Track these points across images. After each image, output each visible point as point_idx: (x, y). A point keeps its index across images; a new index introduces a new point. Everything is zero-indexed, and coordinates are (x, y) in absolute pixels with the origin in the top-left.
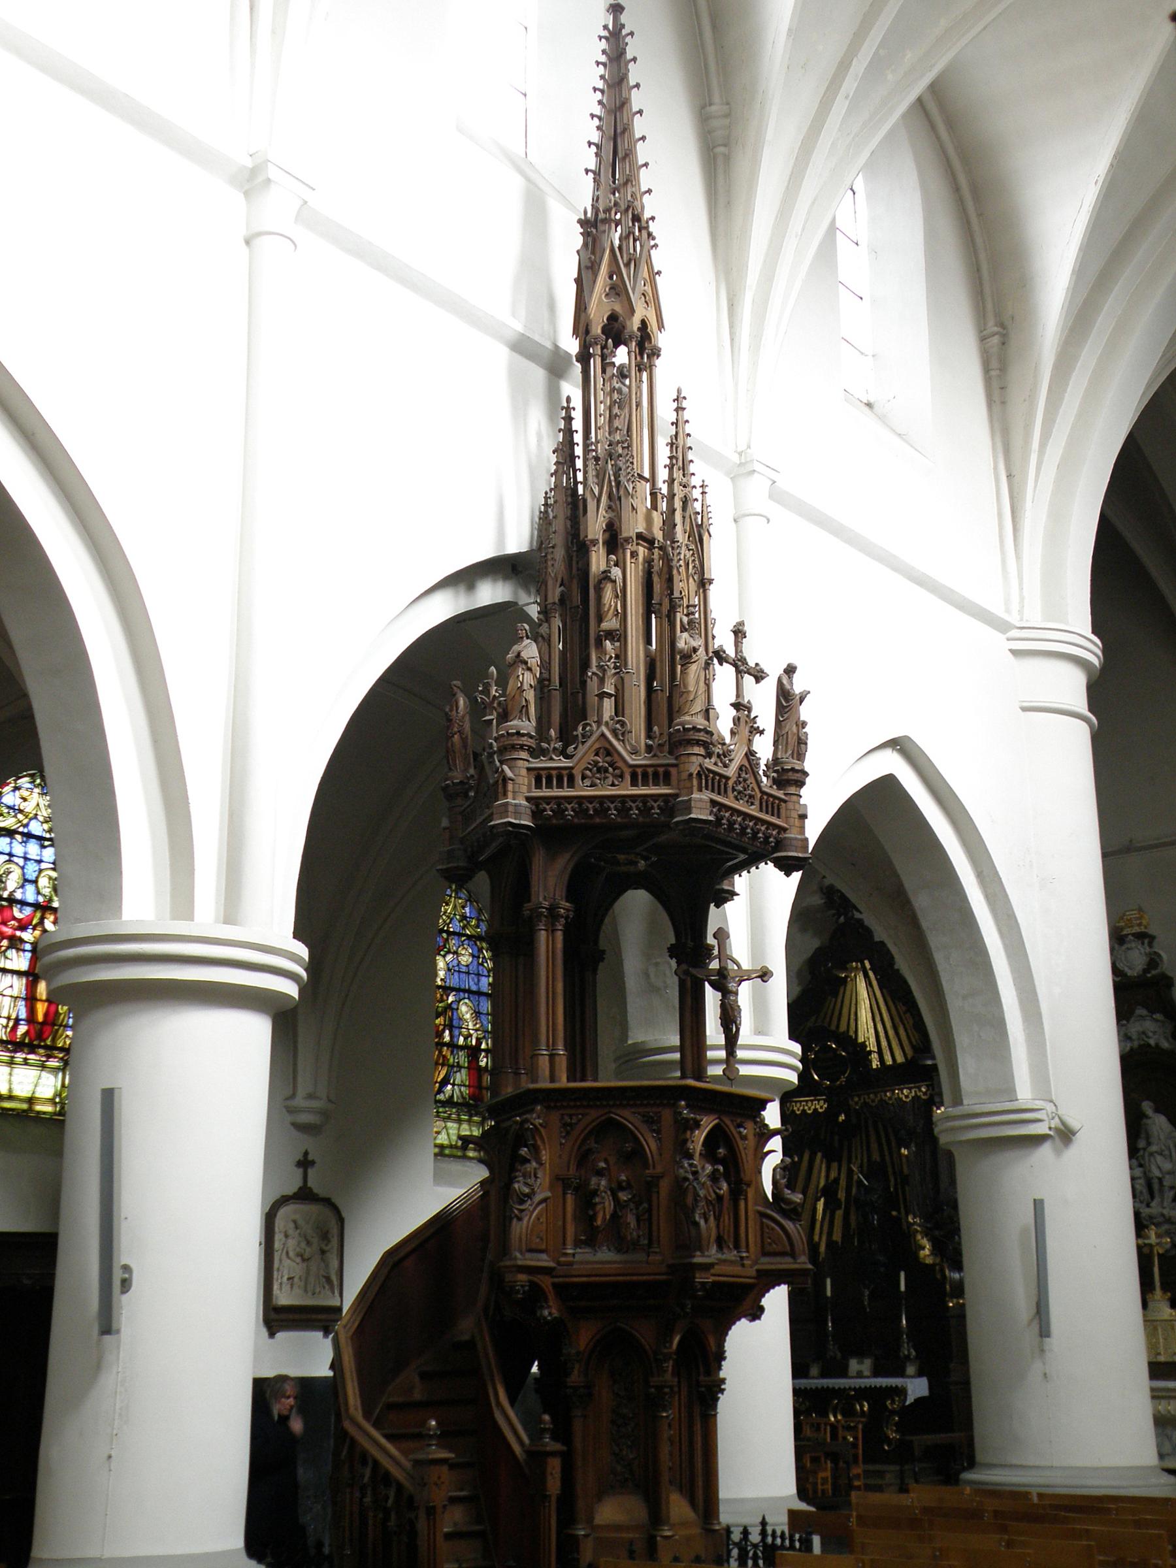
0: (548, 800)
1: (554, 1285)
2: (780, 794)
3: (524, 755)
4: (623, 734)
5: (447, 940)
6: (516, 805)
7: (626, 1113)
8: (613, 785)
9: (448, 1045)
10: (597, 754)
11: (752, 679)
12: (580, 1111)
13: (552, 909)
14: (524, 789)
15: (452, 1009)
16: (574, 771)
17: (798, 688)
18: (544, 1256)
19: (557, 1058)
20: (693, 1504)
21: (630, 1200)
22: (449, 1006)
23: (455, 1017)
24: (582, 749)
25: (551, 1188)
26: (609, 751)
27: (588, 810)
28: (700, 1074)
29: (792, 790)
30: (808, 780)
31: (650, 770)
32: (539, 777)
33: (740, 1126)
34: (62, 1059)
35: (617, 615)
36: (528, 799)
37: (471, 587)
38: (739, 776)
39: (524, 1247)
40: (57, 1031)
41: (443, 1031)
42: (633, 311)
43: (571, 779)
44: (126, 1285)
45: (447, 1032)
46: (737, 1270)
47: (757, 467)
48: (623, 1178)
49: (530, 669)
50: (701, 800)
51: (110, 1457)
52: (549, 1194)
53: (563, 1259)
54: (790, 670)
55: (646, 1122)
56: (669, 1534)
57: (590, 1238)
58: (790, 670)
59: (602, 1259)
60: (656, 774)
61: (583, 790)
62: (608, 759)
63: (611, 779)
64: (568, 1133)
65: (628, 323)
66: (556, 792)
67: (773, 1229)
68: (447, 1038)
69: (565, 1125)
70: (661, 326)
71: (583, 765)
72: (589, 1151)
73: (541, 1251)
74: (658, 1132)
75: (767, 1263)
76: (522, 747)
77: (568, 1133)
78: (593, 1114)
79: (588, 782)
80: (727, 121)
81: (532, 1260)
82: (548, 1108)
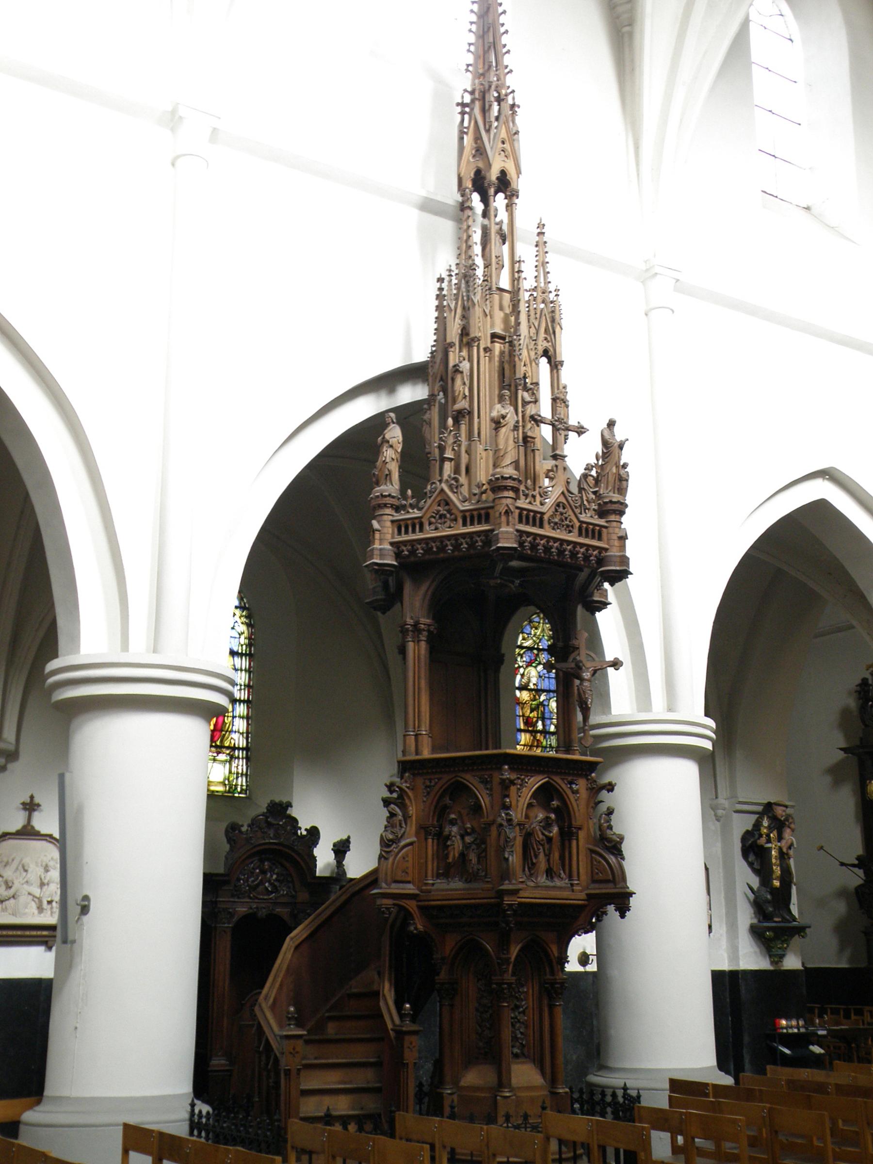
0: (404, 543)
1: (419, 907)
2: (602, 522)
3: (388, 511)
4: (457, 488)
5: (537, 655)
6: (381, 550)
7: (468, 776)
8: (450, 527)
9: (541, 732)
10: (439, 505)
11: (576, 434)
12: (437, 776)
13: (416, 625)
14: (389, 537)
15: (544, 706)
16: (423, 520)
17: (619, 436)
18: (411, 886)
19: (420, 737)
20: (543, 1074)
21: (473, 842)
22: (541, 704)
23: (546, 711)
24: (429, 501)
25: (417, 834)
26: (447, 502)
27: (432, 547)
29: (613, 517)
30: (627, 510)
31: (475, 513)
32: (400, 526)
33: (571, 783)
34: (229, 754)
35: (465, 397)
36: (392, 544)
37: (392, 391)
38: (556, 511)
39: (389, 878)
40: (224, 735)
41: (537, 722)
42: (489, 166)
43: (421, 526)
44: (85, 910)
45: (540, 723)
46: (566, 894)
47: (657, 270)
48: (469, 826)
49: (391, 446)
50: (507, 532)
51: (76, 1028)
52: (414, 839)
53: (424, 888)
54: (611, 424)
55: (482, 782)
56: (508, 1094)
57: (446, 872)
58: (611, 424)
59: (452, 888)
60: (480, 516)
61: (547, 531)
62: (447, 507)
63: (448, 522)
64: (428, 793)
65: (488, 175)
66: (411, 537)
67: (599, 862)
68: (540, 726)
69: (427, 787)
70: (519, 172)
71: (428, 515)
72: (445, 807)
73: (409, 882)
74: (491, 789)
75: (596, 889)
76: (385, 505)
77: (428, 793)
78: (446, 778)
79: (433, 527)
80: (629, 6)
81: (395, 889)
82: (414, 775)
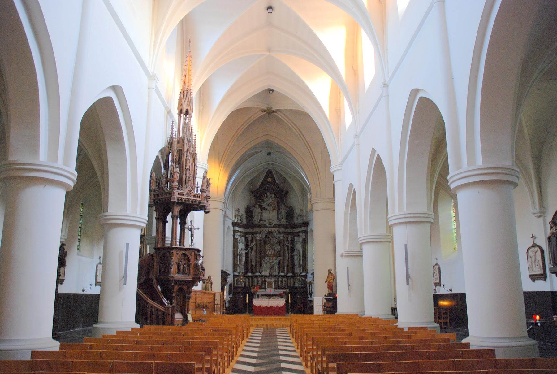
28: (176, 245)
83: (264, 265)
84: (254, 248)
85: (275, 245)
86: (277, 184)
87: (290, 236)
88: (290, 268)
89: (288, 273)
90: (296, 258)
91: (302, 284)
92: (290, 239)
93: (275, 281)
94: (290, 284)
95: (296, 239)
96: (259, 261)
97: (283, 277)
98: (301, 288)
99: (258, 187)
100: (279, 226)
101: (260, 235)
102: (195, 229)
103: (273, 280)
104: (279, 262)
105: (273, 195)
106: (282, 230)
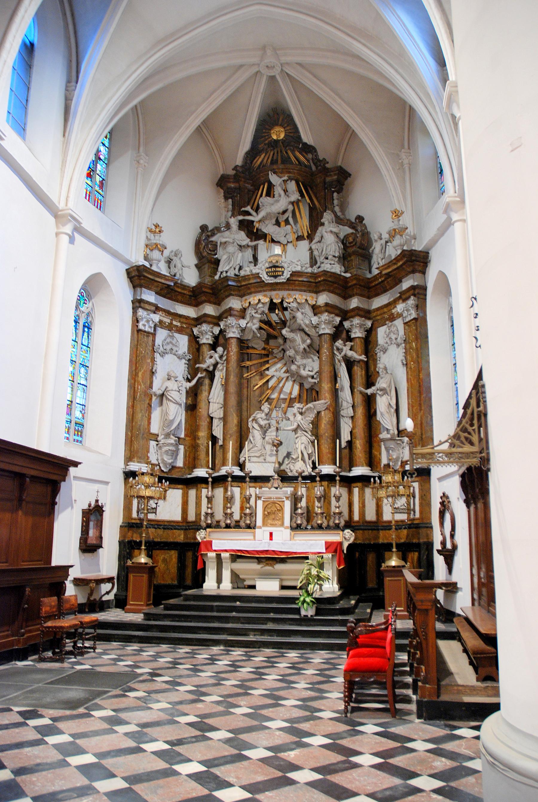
83: (256, 434)
84: (219, 375)
85: (299, 361)
86: (308, 149)
87: (356, 321)
88: (359, 445)
89: (351, 465)
90: (383, 404)
91: (409, 510)
92: (357, 333)
93: (296, 500)
94: (362, 513)
95: (382, 332)
96: (234, 420)
97: (330, 479)
98: (400, 525)
99: (239, 161)
100: (316, 282)
101: (243, 323)
102: (167, 399)
103: (289, 490)
104: (316, 423)
105: (292, 186)
106: (323, 299)
